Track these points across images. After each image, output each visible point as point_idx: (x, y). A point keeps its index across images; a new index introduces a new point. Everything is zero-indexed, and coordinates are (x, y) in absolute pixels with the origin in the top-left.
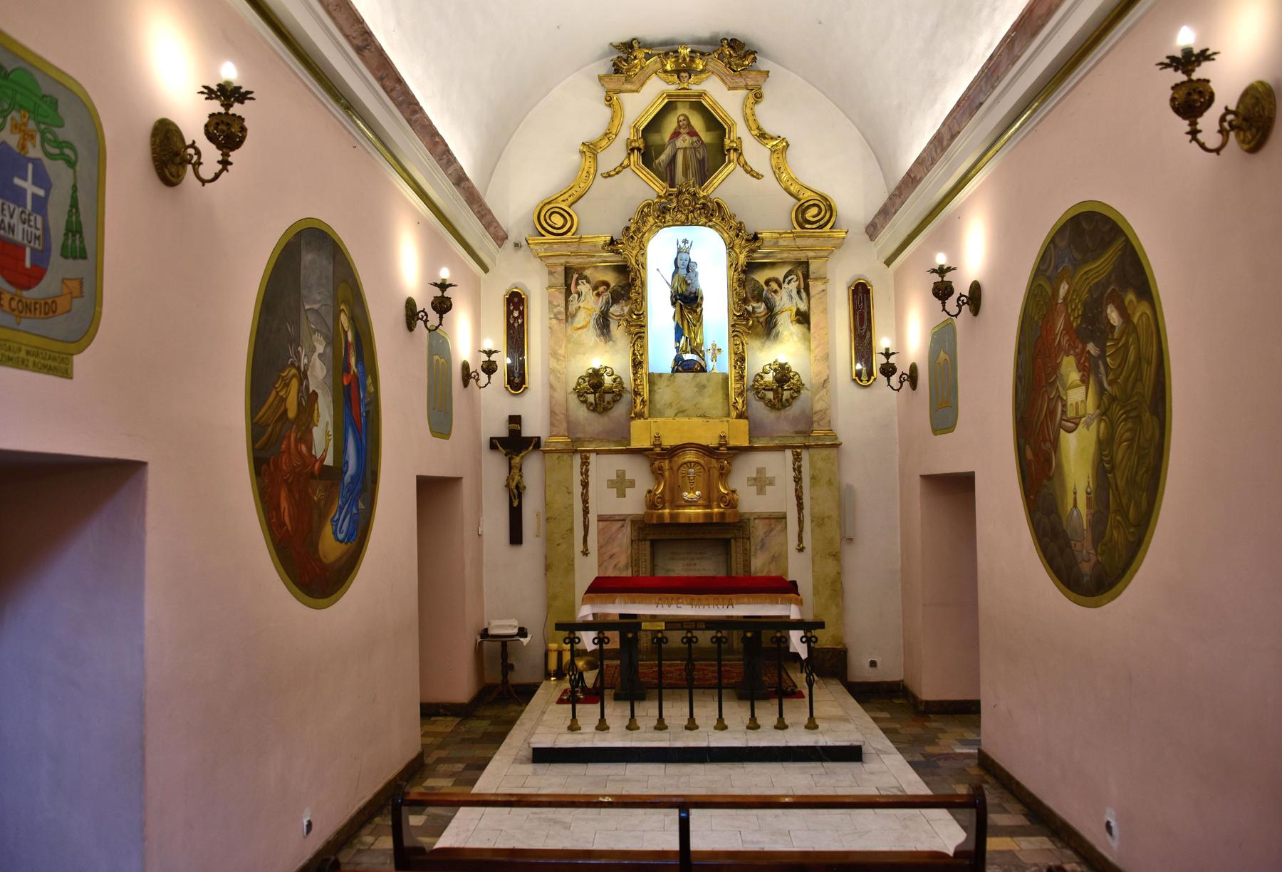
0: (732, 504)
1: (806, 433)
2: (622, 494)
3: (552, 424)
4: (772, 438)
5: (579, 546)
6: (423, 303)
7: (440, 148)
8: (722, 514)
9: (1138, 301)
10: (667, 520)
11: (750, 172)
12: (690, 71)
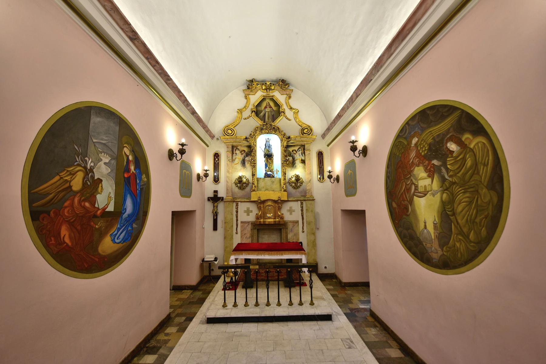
0: (282, 218)
1: (305, 196)
2: (248, 215)
3: (227, 193)
4: (294, 198)
5: (235, 231)
6: (176, 151)
7: (183, 98)
8: (279, 221)
9: (474, 138)
10: (262, 223)
11: (288, 119)
12: (270, 89)
